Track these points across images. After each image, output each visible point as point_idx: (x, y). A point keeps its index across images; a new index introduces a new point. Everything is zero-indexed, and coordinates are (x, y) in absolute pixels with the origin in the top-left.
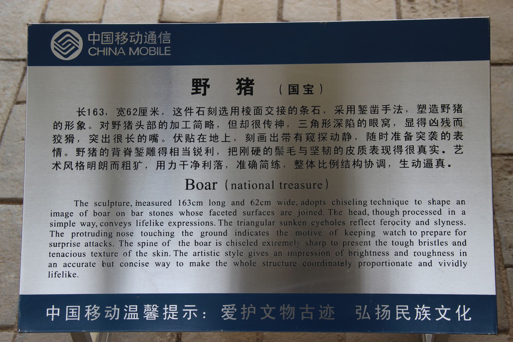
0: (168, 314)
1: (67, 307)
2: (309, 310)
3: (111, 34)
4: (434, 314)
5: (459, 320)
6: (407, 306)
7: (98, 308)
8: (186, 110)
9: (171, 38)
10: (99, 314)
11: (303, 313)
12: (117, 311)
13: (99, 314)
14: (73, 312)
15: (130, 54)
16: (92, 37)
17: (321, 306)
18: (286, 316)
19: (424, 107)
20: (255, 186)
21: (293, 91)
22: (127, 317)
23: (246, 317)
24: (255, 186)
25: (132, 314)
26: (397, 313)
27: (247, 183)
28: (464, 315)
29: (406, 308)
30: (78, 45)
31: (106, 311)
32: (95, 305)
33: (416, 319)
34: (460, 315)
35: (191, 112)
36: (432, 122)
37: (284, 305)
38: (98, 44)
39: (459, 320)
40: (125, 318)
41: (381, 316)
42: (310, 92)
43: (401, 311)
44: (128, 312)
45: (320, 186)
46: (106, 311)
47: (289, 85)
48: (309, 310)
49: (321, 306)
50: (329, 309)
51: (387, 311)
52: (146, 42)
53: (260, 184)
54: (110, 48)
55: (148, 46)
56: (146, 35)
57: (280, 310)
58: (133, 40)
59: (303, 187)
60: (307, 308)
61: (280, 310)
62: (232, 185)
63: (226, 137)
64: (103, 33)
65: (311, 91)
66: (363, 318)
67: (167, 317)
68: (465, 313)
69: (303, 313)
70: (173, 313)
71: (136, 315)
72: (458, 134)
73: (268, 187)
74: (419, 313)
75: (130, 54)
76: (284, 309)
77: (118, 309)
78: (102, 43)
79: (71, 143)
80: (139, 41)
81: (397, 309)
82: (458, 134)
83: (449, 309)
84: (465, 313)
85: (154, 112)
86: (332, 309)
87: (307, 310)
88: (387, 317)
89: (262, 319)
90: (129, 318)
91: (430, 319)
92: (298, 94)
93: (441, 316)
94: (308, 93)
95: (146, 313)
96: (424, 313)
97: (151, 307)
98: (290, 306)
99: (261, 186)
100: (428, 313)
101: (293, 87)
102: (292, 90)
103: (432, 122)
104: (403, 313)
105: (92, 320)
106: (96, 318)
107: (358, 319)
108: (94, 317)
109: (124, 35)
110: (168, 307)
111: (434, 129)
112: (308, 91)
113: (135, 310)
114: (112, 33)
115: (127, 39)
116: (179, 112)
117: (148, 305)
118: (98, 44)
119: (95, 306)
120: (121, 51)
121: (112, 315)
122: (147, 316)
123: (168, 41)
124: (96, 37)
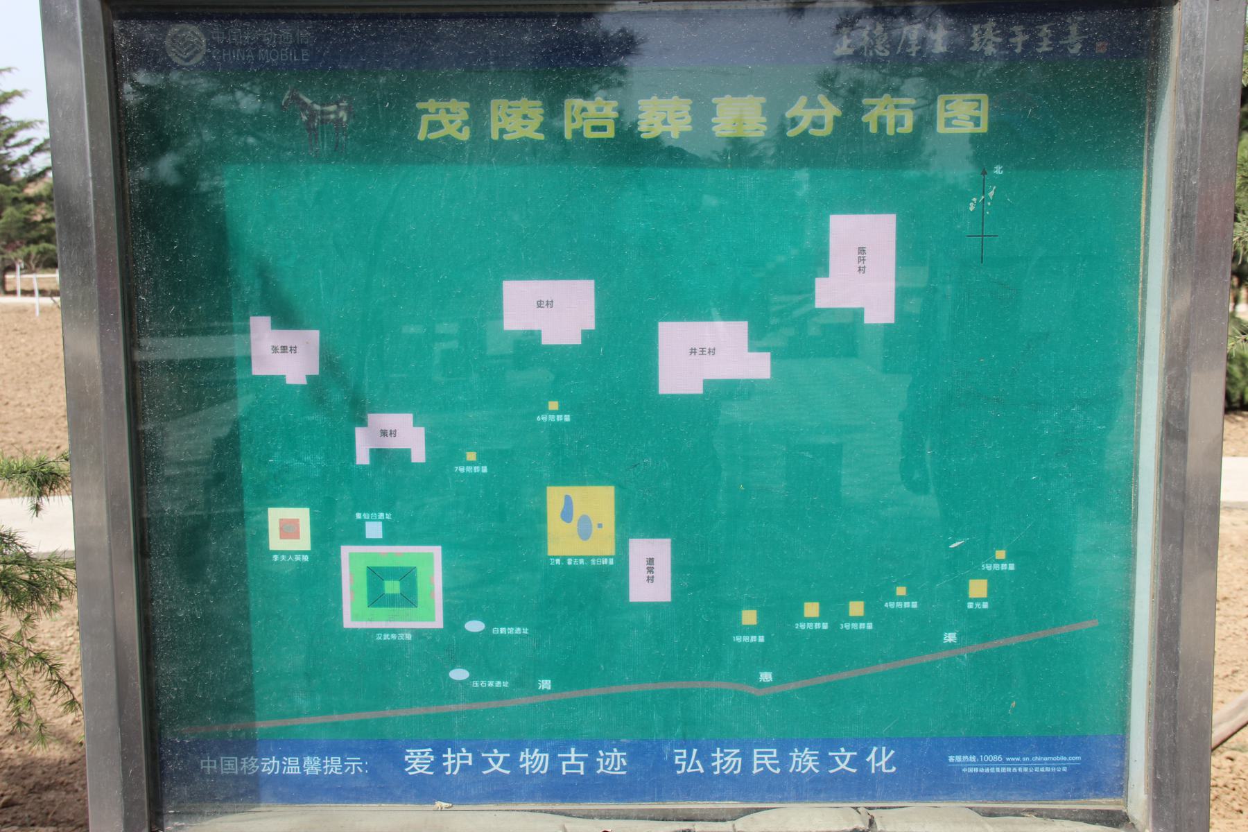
6: (775, 751)
11: (564, 763)
18: (531, 769)
23: (453, 770)
26: (756, 762)
28: (883, 763)
48: (577, 759)
60: (573, 755)
66: (689, 770)
69: (564, 763)
76: (527, 756)
84: (884, 759)
88: (736, 768)
104: (767, 762)
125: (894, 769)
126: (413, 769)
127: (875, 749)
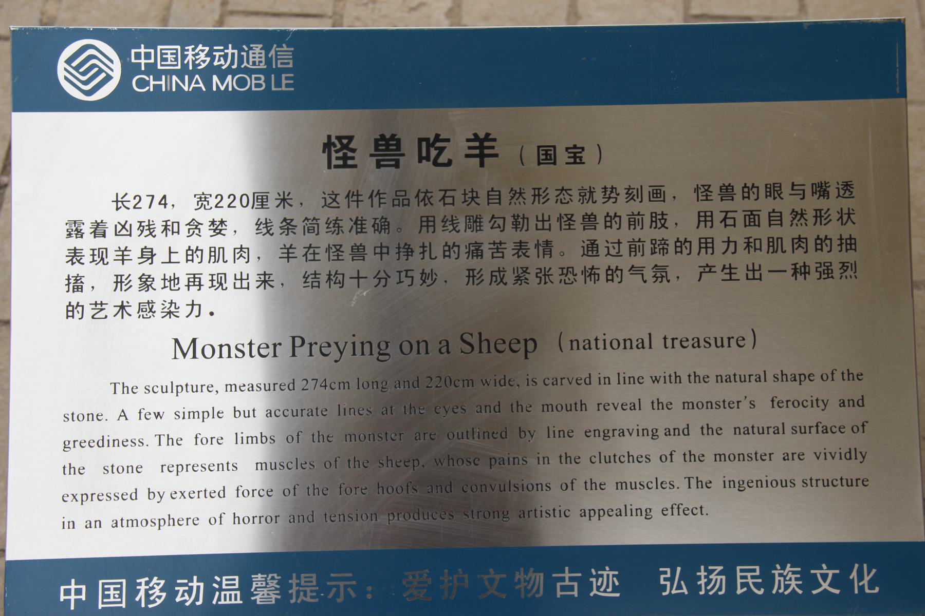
0: (298, 592)
1: (101, 582)
2: (571, 579)
3: (177, 50)
4: (809, 582)
5: (856, 592)
6: (757, 568)
7: (162, 582)
8: (348, 196)
9: (295, 57)
10: (164, 594)
11: (559, 584)
12: (198, 587)
13: (164, 594)
14: (112, 592)
15: (214, 89)
16: (138, 56)
17: (593, 570)
19: (707, 188)
20: (615, 344)
21: (546, 159)
22: (219, 599)
24: (615, 344)
25: (228, 593)
26: (739, 581)
27: (601, 337)
29: (754, 571)
30: (66, 69)
31: (177, 588)
32: (156, 578)
33: (774, 592)
34: (859, 582)
35: (358, 201)
36: (119, 227)
37: (522, 569)
38: (151, 69)
39: (856, 592)
40: (214, 602)
41: (708, 588)
42: (578, 160)
43: (746, 577)
44: (221, 589)
45: (741, 343)
46: (177, 588)
47: (539, 147)
48: (571, 579)
49: (593, 570)
50: (608, 575)
51: (719, 577)
52: (245, 64)
53: (221, 346)
54: (174, 78)
55: (249, 72)
56: (244, 51)
57: (516, 580)
58: (219, 60)
59: (707, 345)
60: (567, 575)
61: (516, 580)
62: (572, 341)
63: (170, 252)
64: (159, 47)
65: (581, 158)
66: (674, 592)
67: (298, 597)
68: (867, 579)
69: (559, 584)
70: (308, 589)
71: (236, 595)
72: (75, 253)
73: (640, 346)
74: (779, 581)
75: (214, 89)
77: (202, 585)
78: (159, 67)
79: (547, 257)
80: (232, 63)
81: (739, 574)
82: (75, 253)
83: (838, 571)
84: (867, 579)
85: (284, 200)
86: (614, 576)
87: (567, 579)
88: (720, 589)
89: (814, 592)
90: (222, 602)
91: (800, 592)
92: (555, 163)
93: (820, 586)
94: (575, 163)
95: (255, 590)
96: (790, 580)
97: (266, 578)
98: (534, 572)
99: (628, 343)
100: (796, 579)
101: (546, 151)
102: (544, 157)
103: (119, 227)
104: (750, 581)
105: (150, 606)
106: (159, 602)
107: (664, 594)
108: (154, 601)
109: (203, 51)
110: (298, 578)
111: (123, 242)
112: (575, 157)
113: (234, 585)
114: (179, 47)
115: (208, 59)
116: (334, 200)
117: (260, 575)
118: (151, 69)
119: (155, 580)
120: (197, 82)
121: (190, 596)
122: (257, 597)
123: (288, 63)
124: (148, 56)
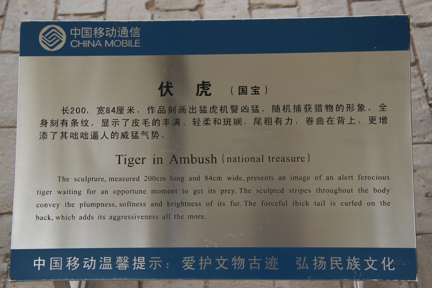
6: (340, 258)
11: (251, 264)
23: (203, 267)
48: (257, 262)
60: (255, 260)
66: (302, 268)
69: (251, 264)
76: (235, 260)
84: (389, 264)
88: (323, 267)
104: (337, 264)
125: (394, 269)
126: (186, 267)
127: (385, 258)
